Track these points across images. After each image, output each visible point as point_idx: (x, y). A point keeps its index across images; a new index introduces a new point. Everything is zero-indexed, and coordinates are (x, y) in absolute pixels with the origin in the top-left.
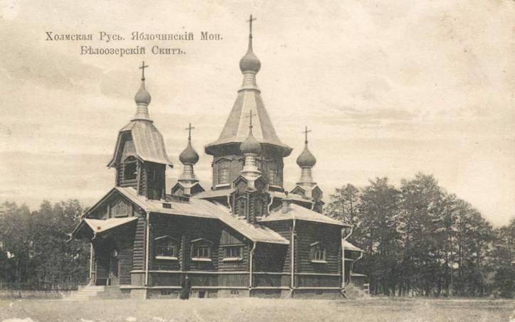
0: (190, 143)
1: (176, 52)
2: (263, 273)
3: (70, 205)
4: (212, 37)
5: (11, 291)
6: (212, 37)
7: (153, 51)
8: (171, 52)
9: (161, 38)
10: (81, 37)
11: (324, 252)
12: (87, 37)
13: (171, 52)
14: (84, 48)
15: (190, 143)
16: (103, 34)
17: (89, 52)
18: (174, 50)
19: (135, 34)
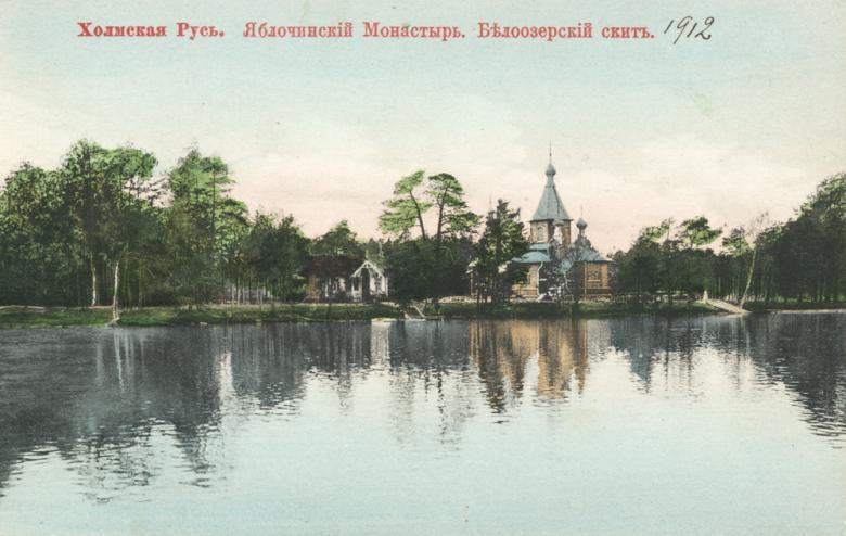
0: (552, 187)
1: (640, 34)
2: (748, 287)
3: (802, 210)
4: (385, 32)
5: (157, 290)
6: (385, 32)
7: (603, 34)
8: (632, 34)
9: (296, 34)
10: (145, 31)
11: (825, 284)
12: (156, 31)
13: (632, 34)
14: (485, 26)
15: (552, 187)
16: (184, 26)
17: (492, 33)
18: (635, 30)
19: (251, 26)
